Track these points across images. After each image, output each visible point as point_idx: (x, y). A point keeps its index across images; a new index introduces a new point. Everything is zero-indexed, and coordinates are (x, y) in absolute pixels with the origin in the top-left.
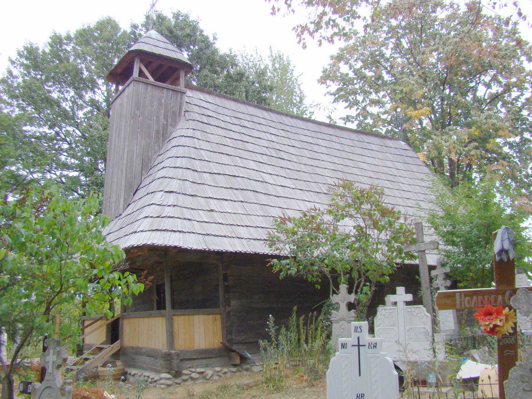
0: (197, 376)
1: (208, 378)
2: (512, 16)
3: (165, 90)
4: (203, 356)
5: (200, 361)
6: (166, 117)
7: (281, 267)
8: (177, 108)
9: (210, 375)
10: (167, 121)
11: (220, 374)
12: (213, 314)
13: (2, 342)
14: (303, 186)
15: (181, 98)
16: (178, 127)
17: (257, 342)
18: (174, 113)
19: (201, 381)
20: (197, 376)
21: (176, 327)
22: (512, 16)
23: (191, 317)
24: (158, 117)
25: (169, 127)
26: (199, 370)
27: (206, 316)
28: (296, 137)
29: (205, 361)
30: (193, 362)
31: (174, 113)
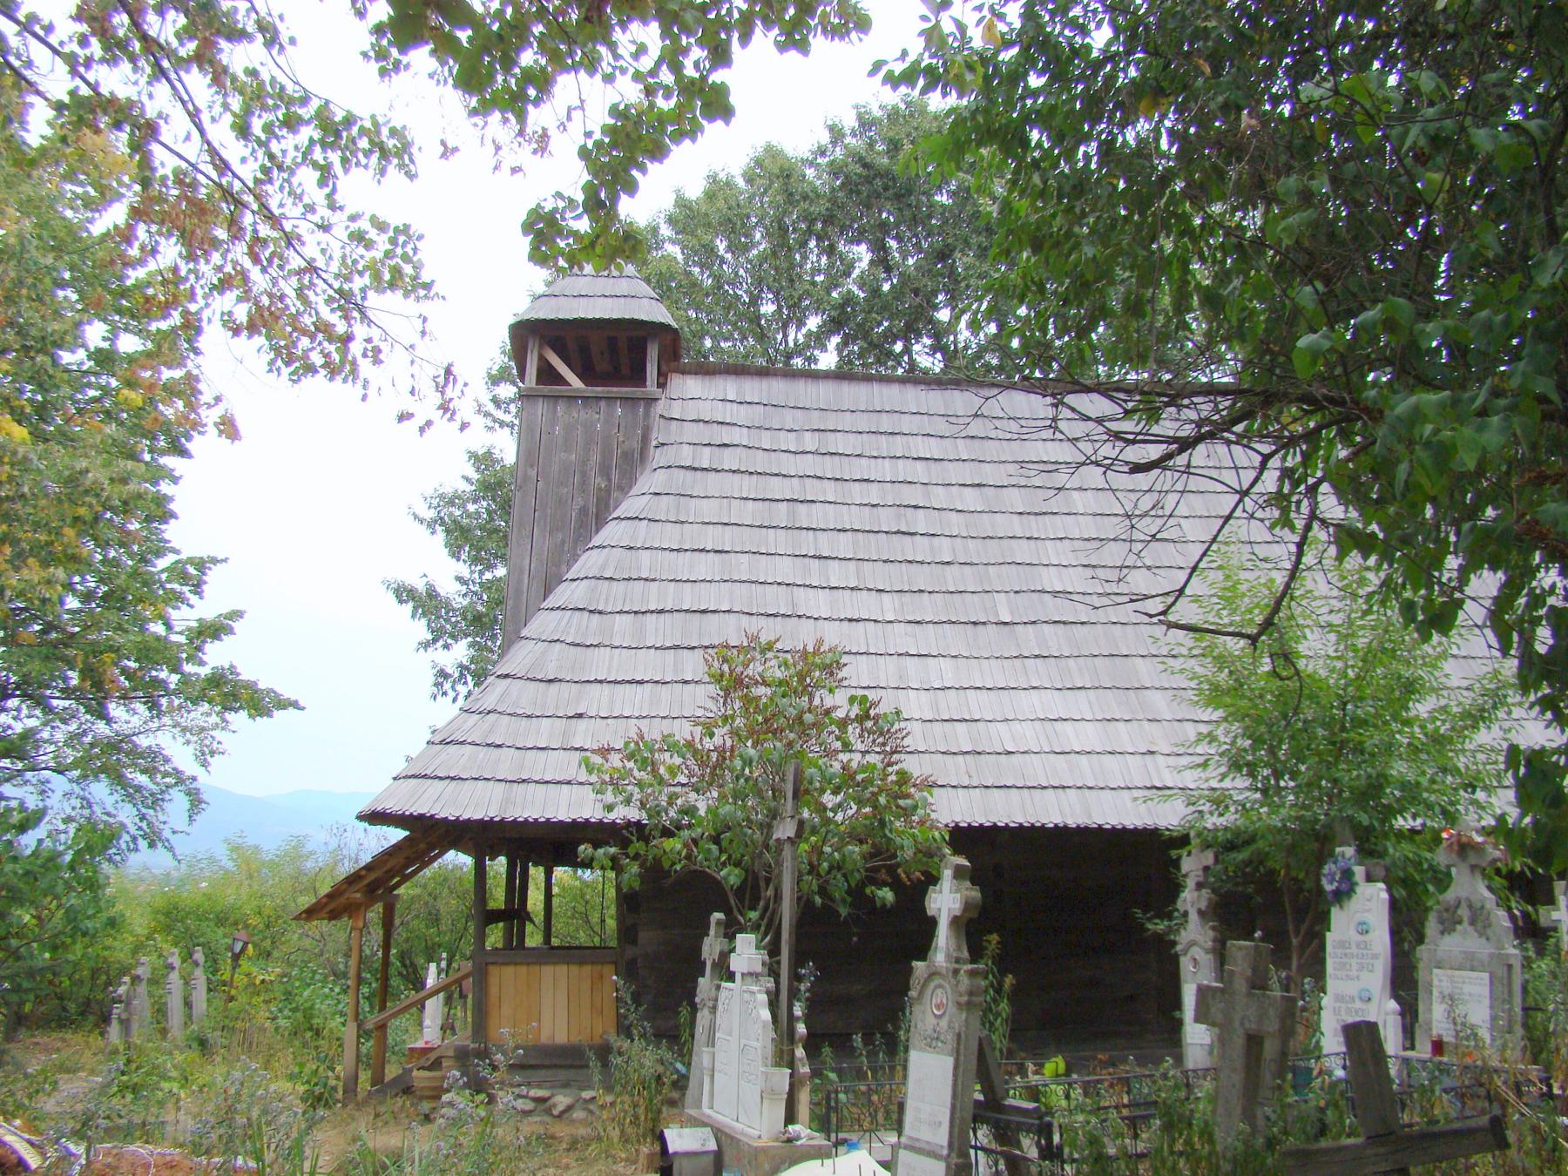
0: (529, 1105)
1: (556, 1112)
2: (295, 705)
3: (603, 404)
4: (569, 1062)
5: (550, 1072)
6: (605, 471)
7: (15, 1008)
8: (636, 445)
9: (561, 1108)
10: (609, 480)
11: (591, 1107)
12: (593, 963)
13: (849, 899)
14: (928, 608)
15: (647, 414)
16: (635, 490)
17: (849, 1035)
18: (627, 456)
19: (538, 1119)
20: (529, 1105)
21: (494, 990)
22: (295, 705)
23: (536, 968)
24: (584, 474)
25: (615, 494)
26: (534, 1093)
27: (574, 969)
28: (873, 494)
29: (563, 1075)
30: (529, 1072)
31: (627, 456)
